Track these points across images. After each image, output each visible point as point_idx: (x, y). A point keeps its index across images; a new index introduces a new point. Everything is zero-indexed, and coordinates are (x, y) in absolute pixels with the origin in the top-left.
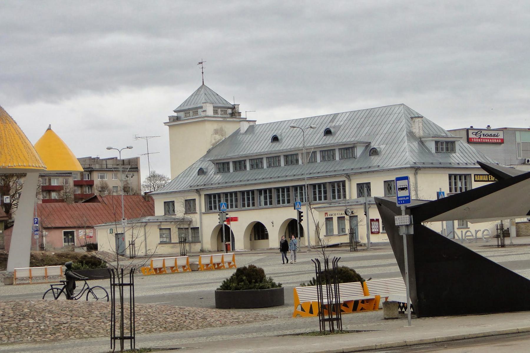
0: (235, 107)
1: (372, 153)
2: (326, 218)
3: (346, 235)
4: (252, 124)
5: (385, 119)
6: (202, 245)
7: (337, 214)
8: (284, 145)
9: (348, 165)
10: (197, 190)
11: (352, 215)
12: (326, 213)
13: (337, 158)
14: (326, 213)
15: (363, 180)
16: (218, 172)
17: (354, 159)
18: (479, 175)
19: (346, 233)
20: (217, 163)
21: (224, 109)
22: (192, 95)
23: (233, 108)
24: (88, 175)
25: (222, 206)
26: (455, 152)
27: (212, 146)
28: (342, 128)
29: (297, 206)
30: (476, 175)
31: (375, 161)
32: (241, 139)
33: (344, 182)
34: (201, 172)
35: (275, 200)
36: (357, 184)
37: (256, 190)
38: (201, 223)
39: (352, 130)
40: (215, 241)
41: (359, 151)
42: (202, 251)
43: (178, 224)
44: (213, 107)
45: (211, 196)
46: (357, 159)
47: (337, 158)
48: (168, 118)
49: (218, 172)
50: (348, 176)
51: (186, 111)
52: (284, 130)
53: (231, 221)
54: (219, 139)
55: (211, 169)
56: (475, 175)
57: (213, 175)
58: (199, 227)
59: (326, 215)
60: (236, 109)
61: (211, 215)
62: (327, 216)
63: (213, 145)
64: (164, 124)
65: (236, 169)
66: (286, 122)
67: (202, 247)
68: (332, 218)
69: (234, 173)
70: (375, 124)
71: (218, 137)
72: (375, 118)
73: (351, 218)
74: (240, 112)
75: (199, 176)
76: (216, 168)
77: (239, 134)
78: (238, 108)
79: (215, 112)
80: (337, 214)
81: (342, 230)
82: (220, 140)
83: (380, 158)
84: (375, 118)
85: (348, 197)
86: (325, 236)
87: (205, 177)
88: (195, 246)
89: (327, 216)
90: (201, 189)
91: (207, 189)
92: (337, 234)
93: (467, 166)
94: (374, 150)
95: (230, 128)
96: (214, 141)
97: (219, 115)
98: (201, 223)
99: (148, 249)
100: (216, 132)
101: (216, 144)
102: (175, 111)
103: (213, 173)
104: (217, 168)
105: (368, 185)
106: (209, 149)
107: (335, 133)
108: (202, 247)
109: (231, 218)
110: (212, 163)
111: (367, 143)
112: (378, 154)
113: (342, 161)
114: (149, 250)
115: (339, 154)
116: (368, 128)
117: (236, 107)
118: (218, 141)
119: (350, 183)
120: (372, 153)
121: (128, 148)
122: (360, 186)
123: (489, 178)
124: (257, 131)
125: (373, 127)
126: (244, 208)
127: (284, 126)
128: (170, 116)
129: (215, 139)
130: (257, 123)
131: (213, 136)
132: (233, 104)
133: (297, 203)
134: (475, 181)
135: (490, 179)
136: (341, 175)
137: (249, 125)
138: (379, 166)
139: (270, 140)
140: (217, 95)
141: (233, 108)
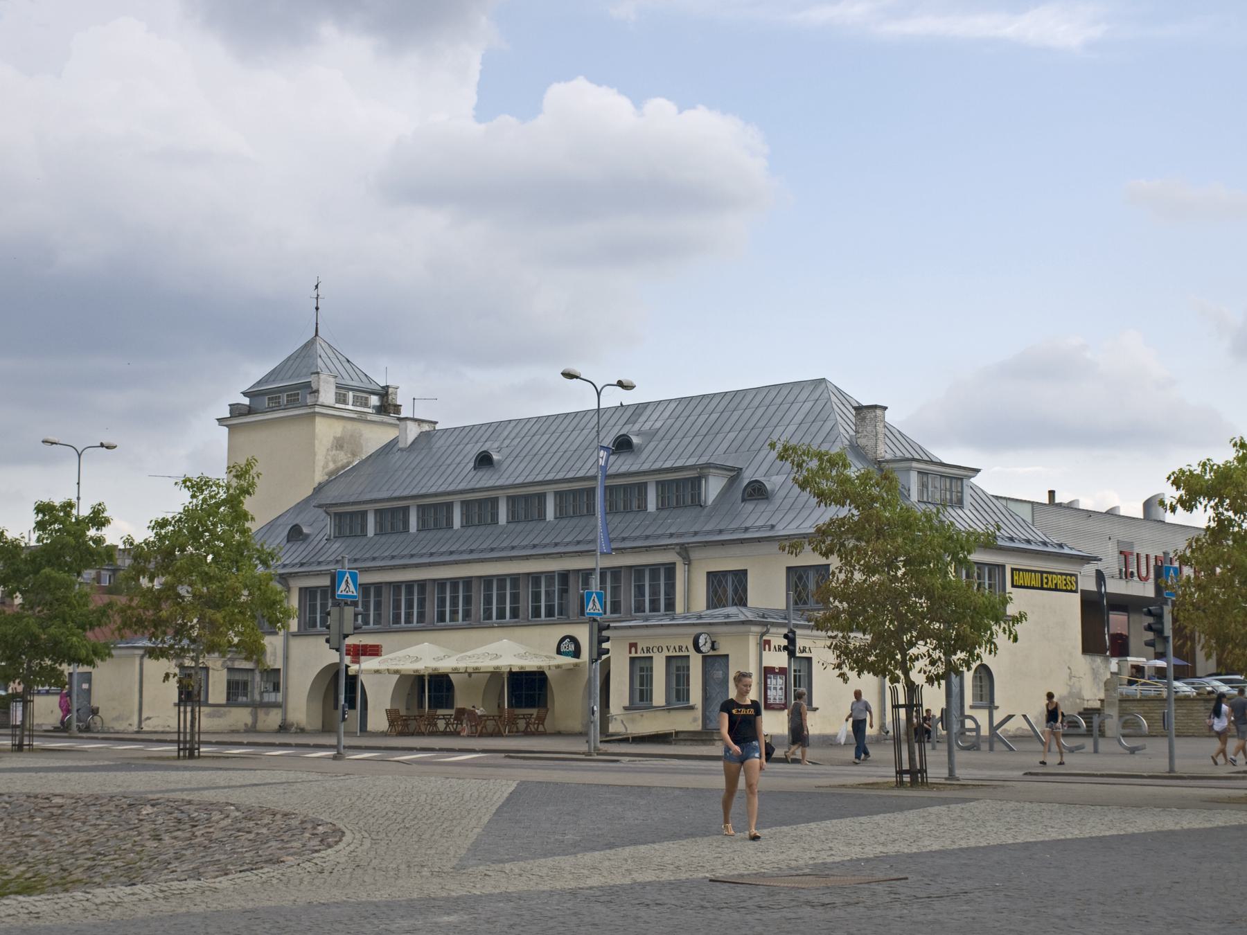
0: (387, 392)
1: (751, 495)
2: (630, 658)
3: (692, 708)
4: (426, 428)
5: (780, 414)
6: (285, 713)
7: (665, 649)
8: (506, 475)
9: (683, 523)
10: (281, 575)
11: (712, 653)
12: (633, 645)
13: (652, 506)
14: (633, 645)
15: (727, 563)
16: (337, 535)
17: (699, 509)
18: (1023, 570)
19: (691, 703)
20: (335, 514)
21: (361, 395)
22: (289, 358)
23: (384, 393)
24: (110, 576)
25: (344, 584)
26: (961, 508)
27: (326, 477)
28: (661, 433)
29: (591, 605)
30: (1016, 570)
31: (756, 517)
32: (396, 462)
33: (670, 569)
34: (296, 534)
35: (478, 607)
36: (709, 573)
37: (429, 580)
38: (286, 658)
39: (687, 440)
40: (318, 707)
41: (713, 488)
42: (284, 728)
43: (229, 659)
44: (337, 387)
45: (316, 592)
46: (706, 510)
47: (652, 506)
48: (229, 407)
49: (337, 535)
50: (684, 551)
51: (273, 394)
52: (507, 442)
53: (362, 655)
54: (345, 461)
55: (319, 526)
56: (1013, 570)
57: (324, 542)
58: (279, 670)
59: (633, 649)
60: (390, 398)
61: (311, 640)
62: (636, 652)
63: (330, 474)
64: (217, 423)
65: (381, 529)
66: (513, 424)
67: (284, 720)
68: (651, 658)
69: (377, 538)
70: (750, 425)
71: (343, 458)
72: (749, 412)
73: (709, 660)
74: (398, 403)
75: (289, 545)
76: (332, 526)
77: (395, 449)
78: (396, 394)
79: (341, 399)
80: (665, 649)
81: (678, 692)
82: (348, 463)
83: (771, 507)
84: (749, 412)
85: (679, 607)
86: (625, 708)
87: (304, 546)
88: (267, 714)
89: (636, 652)
90: (291, 573)
91: (307, 574)
92: (663, 703)
93: (1013, 545)
94: (757, 485)
95: (376, 437)
96: (331, 466)
97: (350, 407)
98: (286, 658)
99: (144, 716)
100: (339, 444)
101: (339, 471)
102: (245, 394)
103: (326, 537)
104: (335, 525)
105: (740, 577)
106: (320, 484)
107: (641, 449)
108: (284, 720)
109: (362, 646)
110: (324, 514)
111: (731, 469)
112: (767, 498)
113: (664, 513)
114: (148, 718)
115: (657, 496)
116: (732, 435)
117: (390, 390)
118: (343, 467)
119: (689, 571)
120: (751, 495)
121: (102, 445)
122: (715, 579)
123: (1045, 580)
124: (438, 445)
125: (744, 433)
126: (398, 626)
127: (506, 433)
128: (234, 405)
129: (334, 462)
130: (438, 427)
131: (330, 453)
132: (384, 385)
133: (590, 595)
134: (1013, 586)
135: (1047, 583)
136: (665, 548)
137: (419, 431)
138: (773, 527)
139: (472, 464)
140: (348, 361)
141: (384, 393)
